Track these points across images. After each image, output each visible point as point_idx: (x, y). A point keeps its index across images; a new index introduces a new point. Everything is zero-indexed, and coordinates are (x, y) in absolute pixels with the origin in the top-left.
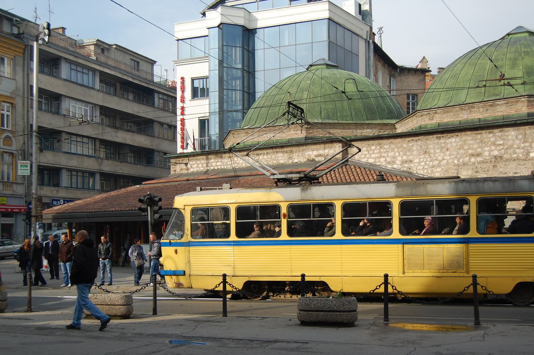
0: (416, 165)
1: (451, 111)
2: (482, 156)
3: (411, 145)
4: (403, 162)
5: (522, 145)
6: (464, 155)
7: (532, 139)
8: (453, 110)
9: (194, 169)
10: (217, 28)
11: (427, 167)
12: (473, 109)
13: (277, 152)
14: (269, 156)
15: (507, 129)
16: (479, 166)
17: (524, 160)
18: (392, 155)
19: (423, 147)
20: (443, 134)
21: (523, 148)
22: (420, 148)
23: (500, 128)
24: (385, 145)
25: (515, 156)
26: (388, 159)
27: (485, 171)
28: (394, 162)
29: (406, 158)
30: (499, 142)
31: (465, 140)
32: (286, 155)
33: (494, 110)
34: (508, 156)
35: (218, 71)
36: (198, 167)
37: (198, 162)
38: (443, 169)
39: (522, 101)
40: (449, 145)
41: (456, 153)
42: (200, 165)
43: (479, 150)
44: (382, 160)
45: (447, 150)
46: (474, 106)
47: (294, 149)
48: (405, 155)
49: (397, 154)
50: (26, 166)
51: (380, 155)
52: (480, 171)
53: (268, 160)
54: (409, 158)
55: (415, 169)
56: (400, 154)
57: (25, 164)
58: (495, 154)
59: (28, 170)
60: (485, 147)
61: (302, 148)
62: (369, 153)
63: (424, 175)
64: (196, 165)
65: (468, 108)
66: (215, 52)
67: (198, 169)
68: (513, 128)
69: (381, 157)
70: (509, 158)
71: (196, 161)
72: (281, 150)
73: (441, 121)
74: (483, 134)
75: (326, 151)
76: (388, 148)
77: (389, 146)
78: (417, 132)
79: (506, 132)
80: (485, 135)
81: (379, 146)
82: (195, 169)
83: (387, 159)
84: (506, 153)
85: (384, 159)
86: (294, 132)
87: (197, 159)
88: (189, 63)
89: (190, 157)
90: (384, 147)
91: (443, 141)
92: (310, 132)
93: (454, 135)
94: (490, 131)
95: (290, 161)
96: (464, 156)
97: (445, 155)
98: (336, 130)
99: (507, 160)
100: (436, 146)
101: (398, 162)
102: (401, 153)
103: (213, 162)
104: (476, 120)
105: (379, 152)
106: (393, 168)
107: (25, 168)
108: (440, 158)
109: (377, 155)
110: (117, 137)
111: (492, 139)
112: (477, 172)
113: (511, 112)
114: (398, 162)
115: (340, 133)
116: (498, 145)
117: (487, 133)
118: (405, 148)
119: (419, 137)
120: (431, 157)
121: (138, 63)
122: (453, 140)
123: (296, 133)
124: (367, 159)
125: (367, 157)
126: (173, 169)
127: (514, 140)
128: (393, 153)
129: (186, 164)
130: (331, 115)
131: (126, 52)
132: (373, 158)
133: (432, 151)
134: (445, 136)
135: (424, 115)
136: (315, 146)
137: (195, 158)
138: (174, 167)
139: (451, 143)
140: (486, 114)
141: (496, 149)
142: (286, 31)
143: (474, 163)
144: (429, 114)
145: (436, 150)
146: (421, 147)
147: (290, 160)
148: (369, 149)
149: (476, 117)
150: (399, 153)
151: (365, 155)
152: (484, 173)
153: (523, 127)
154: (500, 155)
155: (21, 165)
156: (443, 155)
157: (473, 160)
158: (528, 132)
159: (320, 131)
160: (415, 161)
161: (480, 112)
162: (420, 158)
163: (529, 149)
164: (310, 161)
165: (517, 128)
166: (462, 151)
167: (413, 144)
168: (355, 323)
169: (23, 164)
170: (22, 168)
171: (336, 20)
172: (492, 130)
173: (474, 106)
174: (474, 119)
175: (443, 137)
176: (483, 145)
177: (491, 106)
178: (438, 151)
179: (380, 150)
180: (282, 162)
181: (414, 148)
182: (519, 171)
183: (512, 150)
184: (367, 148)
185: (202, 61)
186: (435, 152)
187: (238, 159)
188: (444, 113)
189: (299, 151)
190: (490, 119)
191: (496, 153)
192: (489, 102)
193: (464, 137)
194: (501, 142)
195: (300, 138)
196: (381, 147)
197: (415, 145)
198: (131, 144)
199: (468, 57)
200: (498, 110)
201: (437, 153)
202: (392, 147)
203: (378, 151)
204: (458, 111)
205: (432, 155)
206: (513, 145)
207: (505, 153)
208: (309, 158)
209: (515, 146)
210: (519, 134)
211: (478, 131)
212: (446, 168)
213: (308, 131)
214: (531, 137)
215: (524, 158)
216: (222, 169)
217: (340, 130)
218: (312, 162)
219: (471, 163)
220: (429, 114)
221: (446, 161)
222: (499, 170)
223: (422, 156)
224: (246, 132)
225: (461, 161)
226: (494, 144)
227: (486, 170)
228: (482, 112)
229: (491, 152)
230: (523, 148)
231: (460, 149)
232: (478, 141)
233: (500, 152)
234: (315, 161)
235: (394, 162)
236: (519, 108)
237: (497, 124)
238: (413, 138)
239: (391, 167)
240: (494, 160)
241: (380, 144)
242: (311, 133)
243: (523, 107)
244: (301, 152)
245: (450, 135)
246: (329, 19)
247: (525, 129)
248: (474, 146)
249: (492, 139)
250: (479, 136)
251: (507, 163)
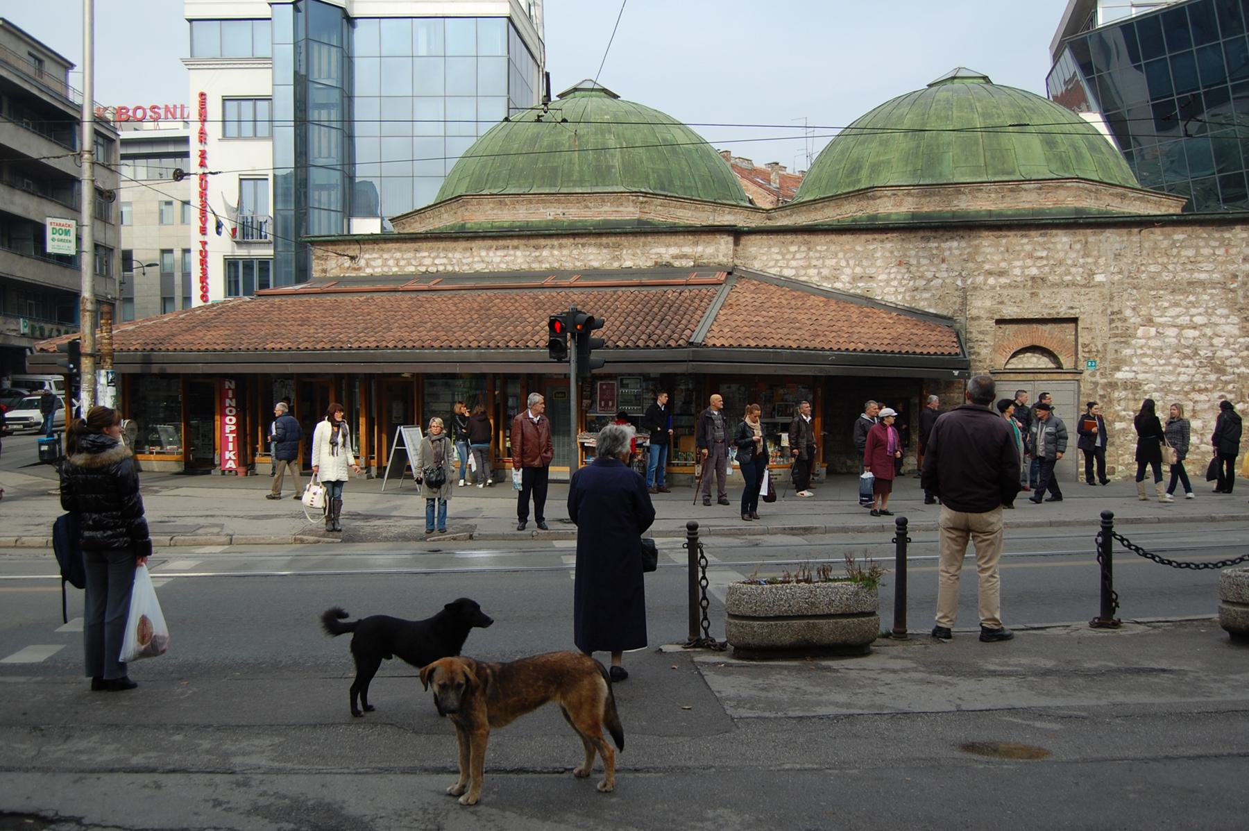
0: (881, 284)
4: (855, 279)
5: (1081, 261)
8: (942, 192)
9: (376, 270)
10: (292, 6)
11: (902, 290)
13: (583, 245)
14: (565, 252)
15: (1054, 232)
16: (1005, 292)
17: (1085, 286)
19: (896, 254)
20: (936, 231)
21: (1083, 266)
24: (818, 245)
25: (1069, 278)
26: (825, 272)
27: (1015, 302)
28: (837, 278)
29: (862, 270)
30: (1039, 254)
31: (977, 246)
32: (605, 251)
33: (1016, 199)
34: (1057, 278)
35: (292, 87)
36: (384, 265)
37: (386, 256)
38: (933, 295)
39: (1068, 187)
40: (947, 253)
41: (960, 268)
42: (391, 262)
43: (1003, 265)
44: (812, 272)
45: (943, 261)
47: (624, 240)
48: (858, 265)
49: (843, 263)
50: (67, 232)
51: (807, 263)
52: (1006, 301)
54: (867, 272)
55: (878, 291)
56: (848, 264)
57: (63, 228)
59: (70, 241)
60: (1013, 259)
61: (642, 239)
62: (784, 259)
63: (897, 305)
64: (379, 262)
66: (286, 53)
67: (386, 269)
68: (1064, 231)
69: (809, 267)
70: (1057, 281)
71: (381, 253)
72: (593, 242)
75: (700, 249)
77: (825, 248)
80: (1015, 240)
82: (379, 270)
83: (821, 270)
85: (816, 271)
87: (383, 250)
88: (217, 66)
89: (364, 244)
91: (936, 245)
92: (645, 210)
94: (1024, 233)
95: (616, 265)
96: (976, 273)
99: (1054, 285)
101: (845, 278)
103: (425, 257)
104: (983, 213)
106: (834, 289)
107: (63, 237)
108: (929, 275)
109: (801, 263)
110: (12, 203)
111: (1028, 248)
112: (1001, 303)
114: (845, 278)
118: (858, 252)
119: (889, 235)
121: (40, 62)
122: (955, 244)
123: (616, 211)
124: (779, 269)
126: (320, 268)
128: (835, 260)
129: (352, 258)
130: (666, 184)
131: (19, 38)
132: (792, 268)
133: (914, 262)
135: (885, 196)
136: (674, 237)
137: (376, 247)
138: (322, 262)
139: (950, 249)
141: (1034, 265)
142: (421, 27)
143: (993, 288)
144: (895, 195)
146: (892, 252)
148: (785, 252)
149: (984, 208)
151: (777, 261)
152: (1014, 304)
153: (1082, 231)
154: (1042, 276)
155: (53, 228)
156: (934, 270)
157: (991, 281)
158: (1091, 239)
160: (880, 278)
162: (890, 273)
163: (1094, 268)
164: (662, 266)
169: (58, 228)
170: (57, 236)
174: (980, 211)
175: (935, 238)
177: (1011, 190)
178: (924, 261)
180: (596, 264)
181: (878, 254)
182: (1076, 304)
184: (780, 249)
185: (229, 66)
186: (918, 262)
187: (488, 254)
190: (1010, 213)
191: (1034, 271)
194: (1044, 254)
196: (809, 249)
198: (37, 220)
199: (896, 103)
200: (1024, 199)
202: (833, 250)
203: (803, 255)
205: (913, 269)
206: (1064, 260)
208: (659, 260)
210: (1075, 242)
212: (940, 293)
214: (1096, 248)
215: (1083, 282)
216: (448, 272)
217: (690, 213)
219: (988, 287)
220: (895, 195)
221: (940, 281)
222: (1043, 301)
223: (894, 270)
225: (969, 282)
226: (1030, 256)
227: (1018, 300)
230: (1083, 266)
235: (837, 278)
236: (1061, 198)
237: (1043, 222)
238: (876, 236)
239: (830, 286)
240: (1030, 283)
241: (808, 243)
243: (1068, 197)
244: (641, 248)
246: (509, 19)
247: (1085, 235)
248: (995, 258)
249: (1028, 248)
250: (1004, 241)
251: (1056, 290)
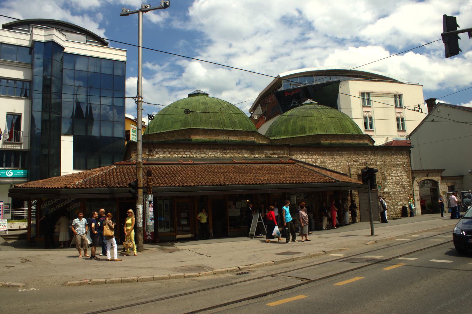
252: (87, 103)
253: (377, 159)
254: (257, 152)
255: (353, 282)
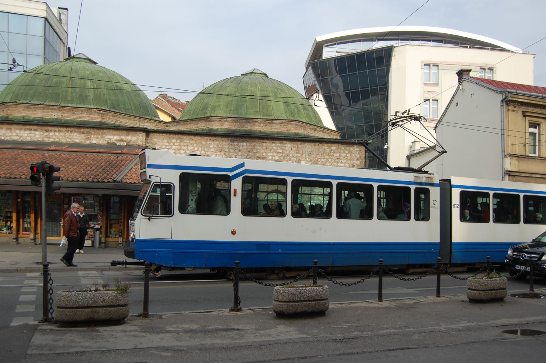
1: (239, 122)
2: (266, 159)
3: (209, 143)
6: (252, 156)
7: (303, 152)
8: (241, 121)
12: (256, 123)
13: (71, 132)
14: (62, 134)
18: (192, 149)
19: (219, 146)
21: (296, 157)
22: (216, 147)
23: (280, 140)
24: (185, 140)
29: (205, 153)
31: (254, 146)
32: (82, 135)
39: (292, 124)
41: (246, 155)
45: (240, 151)
46: (257, 121)
47: (92, 131)
49: (196, 149)
51: (180, 148)
53: (60, 137)
56: (198, 149)
58: (277, 159)
60: (269, 152)
61: (101, 131)
62: (169, 145)
65: (252, 121)
69: (181, 149)
72: (76, 130)
73: (229, 128)
74: (267, 143)
75: (129, 138)
76: (188, 143)
77: (188, 141)
78: (217, 134)
79: (285, 144)
81: (180, 140)
83: (186, 151)
84: (284, 159)
86: (87, 116)
90: (184, 142)
91: (237, 144)
93: (246, 140)
94: (273, 141)
95: (88, 142)
96: (253, 157)
97: (237, 155)
98: (125, 120)
100: (230, 147)
102: (200, 149)
104: (258, 132)
105: (179, 145)
109: (177, 147)
111: (275, 148)
113: (284, 130)
115: (128, 123)
116: (278, 153)
117: (271, 143)
118: (203, 145)
119: (217, 138)
120: (225, 155)
122: (245, 144)
123: (89, 117)
125: (167, 148)
127: (290, 151)
130: (116, 106)
132: (173, 149)
134: (238, 140)
139: (243, 146)
140: (265, 128)
141: (277, 156)
144: (220, 120)
145: (230, 150)
146: (218, 146)
147: (87, 140)
148: (170, 142)
149: (258, 130)
150: (198, 148)
151: (166, 146)
153: (296, 142)
156: (236, 154)
158: (300, 146)
159: (112, 118)
161: (261, 127)
162: (216, 155)
163: (300, 158)
165: (292, 142)
166: (251, 153)
167: (210, 142)
168: (504, 299)
171: (50, 21)
172: (274, 141)
173: (257, 121)
175: (236, 141)
176: (268, 151)
177: (269, 123)
178: (231, 151)
179: (180, 143)
180: (78, 141)
181: (212, 146)
183: (288, 158)
184: (168, 140)
186: (229, 151)
188: (233, 122)
189: (98, 134)
190: (268, 132)
192: (269, 120)
193: (254, 143)
194: (281, 151)
195: (94, 121)
196: (181, 141)
197: (212, 144)
201: (231, 152)
203: (178, 144)
204: (244, 123)
207: (283, 159)
208: (109, 141)
209: (291, 155)
211: (264, 140)
213: (103, 116)
214: (302, 150)
217: (127, 120)
218: (112, 145)
220: (220, 120)
223: (218, 153)
224: (27, 106)
226: (276, 151)
228: (262, 126)
229: (274, 157)
230: (296, 157)
231: (249, 152)
232: (264, 148)
233: (280, 158)
234: (116, 145)
241: (180, 139)
242: (105, 119)
244: (101, 135)
245: (242, 140)
246: (46, 19)
247: (297, 144)
248: (261, 151)
249: (275, 148)
250: (265, 144)
252: (504, 135)
253: (301, 156)
254: (95, 136)
255: (79, 328)
